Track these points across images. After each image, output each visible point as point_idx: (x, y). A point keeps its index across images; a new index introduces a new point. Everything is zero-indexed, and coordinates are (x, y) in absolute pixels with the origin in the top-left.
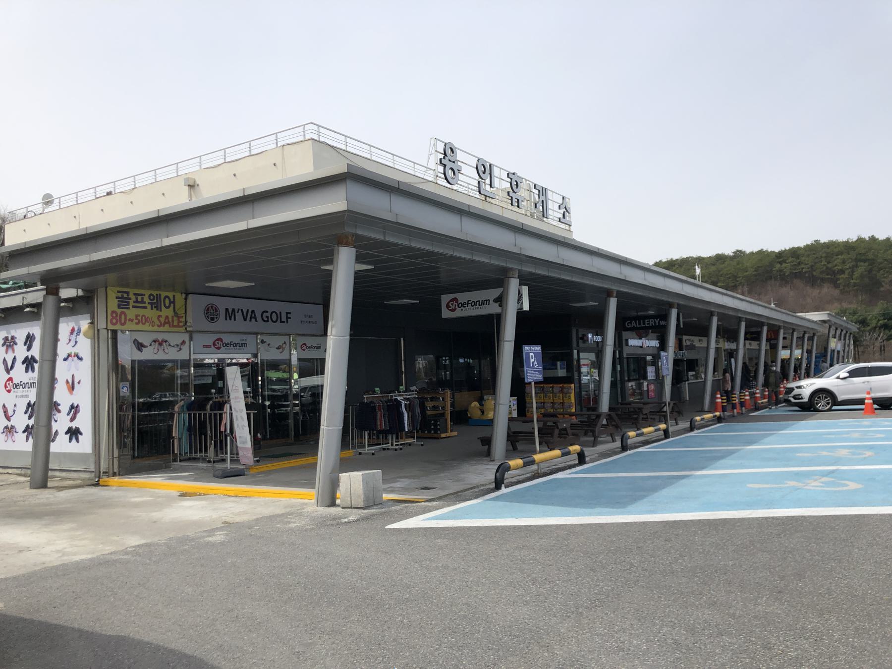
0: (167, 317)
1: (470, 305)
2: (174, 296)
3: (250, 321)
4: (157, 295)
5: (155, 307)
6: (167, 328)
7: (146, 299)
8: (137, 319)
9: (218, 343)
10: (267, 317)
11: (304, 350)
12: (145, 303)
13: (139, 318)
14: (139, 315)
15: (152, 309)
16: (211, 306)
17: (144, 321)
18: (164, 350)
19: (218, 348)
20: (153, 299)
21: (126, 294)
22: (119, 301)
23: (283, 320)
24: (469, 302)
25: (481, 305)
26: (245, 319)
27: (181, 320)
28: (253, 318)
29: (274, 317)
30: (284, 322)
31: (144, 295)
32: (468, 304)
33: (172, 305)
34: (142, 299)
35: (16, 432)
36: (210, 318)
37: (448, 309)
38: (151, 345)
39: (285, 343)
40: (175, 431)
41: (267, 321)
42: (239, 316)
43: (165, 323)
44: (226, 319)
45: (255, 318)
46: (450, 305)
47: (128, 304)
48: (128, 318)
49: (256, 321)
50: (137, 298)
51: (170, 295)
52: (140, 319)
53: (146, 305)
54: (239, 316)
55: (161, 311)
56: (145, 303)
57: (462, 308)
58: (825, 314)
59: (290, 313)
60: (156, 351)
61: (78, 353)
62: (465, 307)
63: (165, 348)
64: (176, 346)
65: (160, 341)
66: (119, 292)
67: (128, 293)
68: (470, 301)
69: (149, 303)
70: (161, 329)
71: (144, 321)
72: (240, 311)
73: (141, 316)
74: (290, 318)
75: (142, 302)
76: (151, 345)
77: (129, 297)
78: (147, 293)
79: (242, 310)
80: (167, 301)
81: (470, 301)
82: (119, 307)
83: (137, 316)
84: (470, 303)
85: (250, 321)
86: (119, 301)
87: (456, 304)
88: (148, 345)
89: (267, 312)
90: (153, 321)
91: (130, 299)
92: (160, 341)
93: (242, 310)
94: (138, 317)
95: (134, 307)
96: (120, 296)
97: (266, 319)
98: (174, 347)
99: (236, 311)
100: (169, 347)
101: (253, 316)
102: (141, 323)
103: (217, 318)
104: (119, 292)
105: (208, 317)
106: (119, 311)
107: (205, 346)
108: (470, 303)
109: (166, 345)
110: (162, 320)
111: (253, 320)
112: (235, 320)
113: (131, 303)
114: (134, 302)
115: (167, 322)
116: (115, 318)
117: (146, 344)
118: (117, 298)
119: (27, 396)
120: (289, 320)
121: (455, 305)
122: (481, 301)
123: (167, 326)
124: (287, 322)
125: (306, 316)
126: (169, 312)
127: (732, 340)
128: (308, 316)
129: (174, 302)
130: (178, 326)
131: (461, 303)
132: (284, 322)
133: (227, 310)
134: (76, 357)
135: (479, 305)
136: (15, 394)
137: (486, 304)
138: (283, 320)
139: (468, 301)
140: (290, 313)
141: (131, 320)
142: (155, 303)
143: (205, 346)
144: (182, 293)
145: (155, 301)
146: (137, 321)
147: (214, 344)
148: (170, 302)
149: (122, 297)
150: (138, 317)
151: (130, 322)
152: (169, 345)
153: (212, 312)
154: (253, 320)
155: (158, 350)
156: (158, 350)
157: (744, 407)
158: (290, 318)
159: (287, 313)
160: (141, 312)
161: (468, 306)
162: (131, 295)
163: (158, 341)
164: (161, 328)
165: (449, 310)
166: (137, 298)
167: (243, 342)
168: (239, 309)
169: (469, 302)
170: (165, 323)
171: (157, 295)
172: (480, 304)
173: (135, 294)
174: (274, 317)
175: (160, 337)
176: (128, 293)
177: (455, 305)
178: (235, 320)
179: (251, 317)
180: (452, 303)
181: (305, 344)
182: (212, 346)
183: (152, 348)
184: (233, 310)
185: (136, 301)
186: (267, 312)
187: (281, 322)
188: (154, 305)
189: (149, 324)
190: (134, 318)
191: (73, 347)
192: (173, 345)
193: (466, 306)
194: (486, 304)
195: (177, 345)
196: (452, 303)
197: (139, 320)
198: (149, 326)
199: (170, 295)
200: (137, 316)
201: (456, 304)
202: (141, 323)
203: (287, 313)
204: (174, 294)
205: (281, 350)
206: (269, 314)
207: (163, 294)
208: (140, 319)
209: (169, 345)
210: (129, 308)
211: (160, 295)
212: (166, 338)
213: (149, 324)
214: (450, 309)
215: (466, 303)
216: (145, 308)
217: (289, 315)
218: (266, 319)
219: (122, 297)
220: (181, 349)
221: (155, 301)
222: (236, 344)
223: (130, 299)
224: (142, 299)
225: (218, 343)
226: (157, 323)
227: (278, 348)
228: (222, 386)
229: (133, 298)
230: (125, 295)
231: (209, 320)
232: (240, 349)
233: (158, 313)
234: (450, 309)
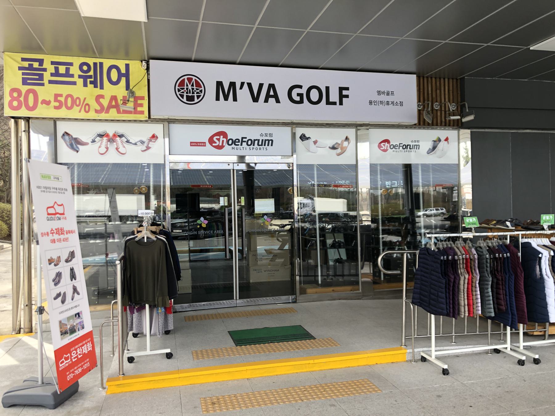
0: (114, 98)
1: (244, 144)
2: (127, 66)
3: (266, 101)
4: (95, 64)
5: (91, 83)
6: (113, 114)
7: (75, 70)
8: (56, 100)
9: (219, 140)
10: (300, 95)
11: (385, 151)
12: (72, 76)
13: (62, 99)
14: (61, 95)
15: (85, 85)
16: (188, 79)
17: (69, 104)
18: (117, 149)
19: (220, 147)
20: (89, 70)
21: (38, 63)
22: (23, 74)
23: (331, 100)
25: (262, 145)
26: (255, 99)
27: (139, 102)
28: (272, 96)
29: (314, 95)
30: (334, 103)
31: (71, 64)
32: (400, 146)
33: (123, 80)
34: (67, 70)
36: (185, 97)
38: (93, 141)
39: (347, 139)
40: (182, 248)
41: (301, 102)
42: (244, 94)
43: (110, 106)
44: (218, 99)
45: (276, 97)
47: (41, 77)
48: (40, 100)
49: (278, 101)
50: (57, 69)
51: (121, 64)
52: (63, 101)
53: (76, 79)
54: (244, 94)
55: (102, 88)
56: (72, 76)
59: (347, 89)
60: (103, 150)
62: (238, 145)
63: (120, 146)
64: (139, 143)
65: (111, 135)
66: (23, 60)
67: (41, 62)
69: (80, 77)
70: (103, 116)
71: (69, 104)
72: (246, 86)
73: (64, 96)
74: (347, 96)
75: (68, 74)
76: (93, 141)
77: (44, 67)
78: (77, 61)
79: (249, 85)
80: (114, 75)
82: (25, 82)
83: (56, 96)
85: (266, 101)
86: (23, 74)
88: (89, 141)
89: (300, 87)
90: (87, 104)
91: (45, 70)
92: (111, 135)
93: (249, 85)
94: (59, 98)
95: (50, 82)
96: (27, 66)
97: (298, 99)
98: (136, 144)
99: (238, 86)
100: (126, 145)
101: (272, 93)
102: (64, 107)
103: (198, 97)
104: (23, 60)
105: (182, 96)
106: (24, 89)
107: (193, 144)
109: (122, 142)
110: (105, 102)
111: (272, 100)
112: (235, 99)
113: (47, 76)
114: (52, 75)
115: (114, 104)
116: (17, 99)
117: (83, 139)
118: (20, 68)
120: (344, 99)
122: (415, 148)
123: (113, 111)
124: (341, 103)
125: (379, 93)
126: (120, 91)
128: (383, 93)
129: (127, 75)
130: (136, 112)
132: (334, 103)
133: (219, 84)
135: (258, 145)
137: (268, 145)
138: (331, 100)
140: (347, 89)
141: (48, 103)
142: (90, 77)
143: (193, 144)
144: (142, 61)
145: (91, 73)
146: (57, 104)
147: (211, 141)
148: (120, 75)
149: (31, 67)
150: (59, 98)
151: (44, 105)
152: (128, 142)
153: (190, 87)
154: (272, 100)
155: (107, 148)
156: (107, 148)
158: (347, 96)
159: (341, 89)
160: (64, 90)
161: (241, 145)
162: (47, 65)
163: (107, 135)
164: (101, 114)
165: (214, 147)
166: (57, 69)
167: (267, 138)
168: (243, 84)
170: (110, 106)
171: (95, 64)
172: (260, 144)
173: (53, 63)
174: (314, 95)
175: (111, 129)
176: (41, 62)
178: (235, 99)
179: (268, 97)
181: (387, 141)
182: (208, 144)
183: (97, 145)
184: (232, 85)
185: (57, 73)
186: (300, 87)
187: (328, 103)
188: (89, 80)
189: (79, 108)
190: (52, 99)
192: (134, 142)
193: (398, 148)
194: (268, 145)
195: (142, 142)
197: (60, 102)
198: (80, 112)
199: (121, 64)
200: (56, 96)
202: (64, 107)
203: (341, 89)
204: (127, 62)
205: (339, 151)
206: (304, 91)
207: (107, 63)
208: (63, 101)
209: (128, 142)
210: (43, 85)
211: (101, 64)
212: (121, 132)
213: (79, 108)
214: (381, 149)
216: (74, 83)
217: (345, 93)
218: (298, 99)
219: (31, 67)
220: (148, 148)
221: (91, 73)
222: (253, 142)
223: (45, 70)
224: (67, 70)
225: (219, 140)
226: (94, 105)
227: (333, 148)
228: (226, 204)
229: (51, 69)
230: (36, 65)
231: (185, 100)
232: (260, 149)
233: (98, 91)
234: (381, 149)
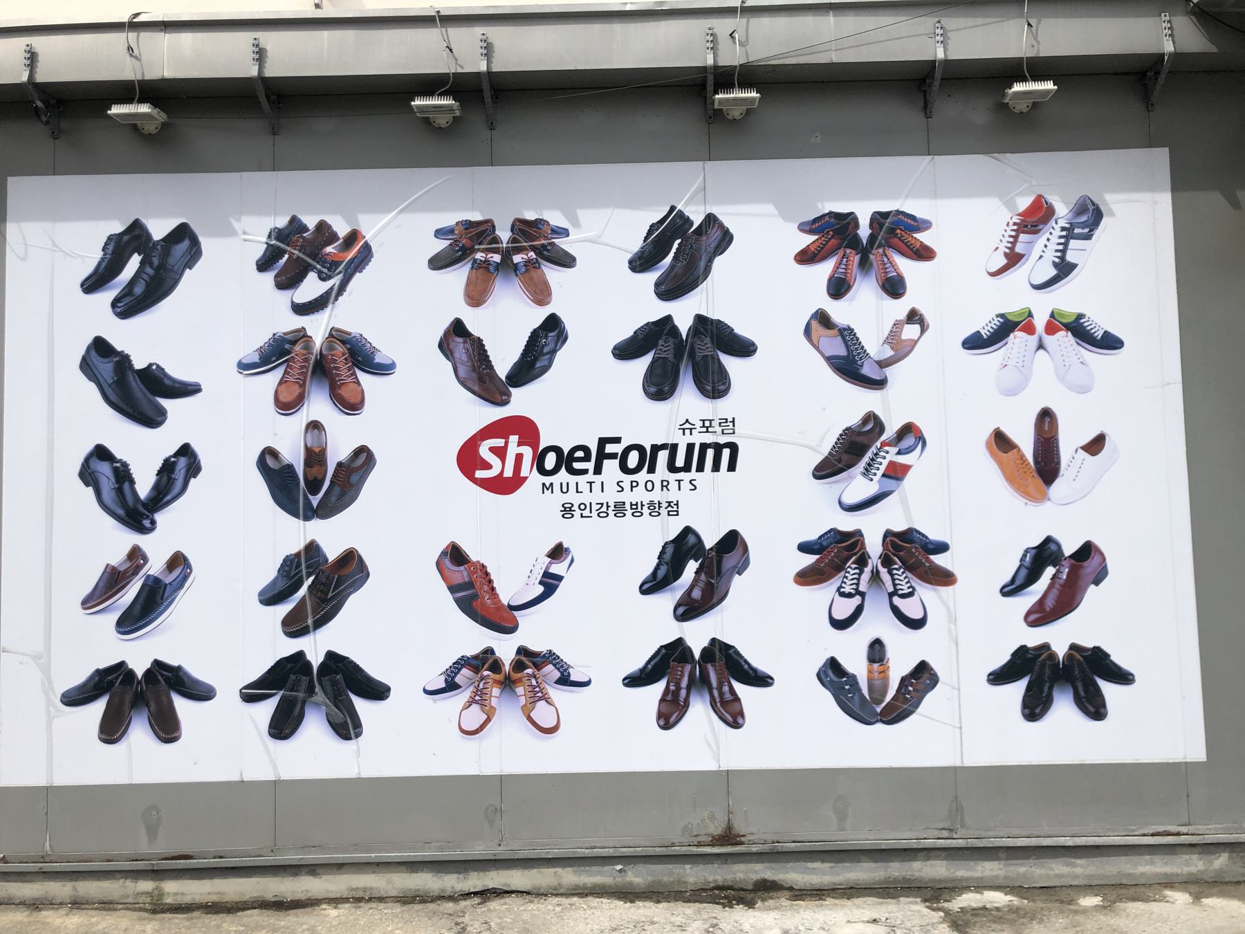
1: (611, 466)
24: (610, 448)
32: (602, 456)
35: (565, 680)
37: (469, 475)
46: (484, 451)
57: (563, 474)
58: (188, 688)
61: (1080, 316)
62: (585, 472)
68: (617, 440)
81: (617, 440)
84: (613, 456)
87: (527, 452)
108: (613, 456)
119: (673, 509)
121: (519, 458)
127: (1027, 711)
131: (557, 450)
134: (1064, 339)
135: (672, 468)
136: (558, 499)
137: (716, 467)
139: (603, 442)
157: (1192, 903)
161: (598, 470)
167: (708, 438)
169: (610, 448)
172: (680, 462)
177: (519, 458)
180: (499, 442)
191: (994, 274)
193: (590, 466)
194: (716, 467)
196: (499, 442)
201: (527, 452)
214: (480, 474)
215: (585, 449)
234: (480, 474)
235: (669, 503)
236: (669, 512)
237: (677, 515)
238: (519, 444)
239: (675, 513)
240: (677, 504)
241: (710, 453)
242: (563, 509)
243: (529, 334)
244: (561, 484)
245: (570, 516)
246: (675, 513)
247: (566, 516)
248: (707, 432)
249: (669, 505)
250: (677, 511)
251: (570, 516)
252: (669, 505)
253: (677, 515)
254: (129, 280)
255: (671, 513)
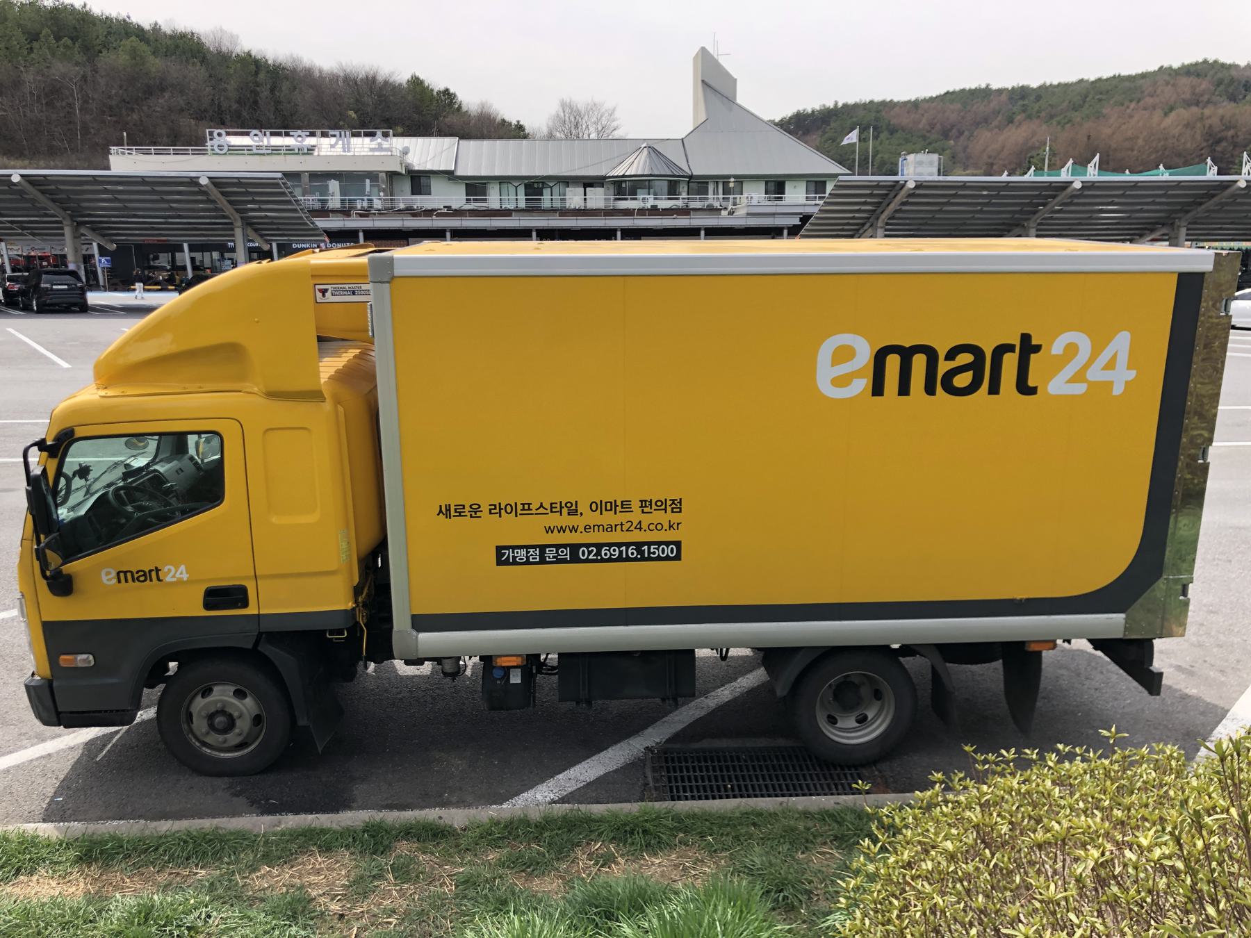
137: (904, 389)
194: (904, 389)
235: (673, 500)
236: (673, 508)
237: (680, 512)
238: (1109, 384)
239: (678, 510)
240: (680, 503)
241: (893, 362)
242: (503, 506)
243: (1211, 59)
244: (441, 506)
245: (473, 507)
246: (678, 510)
247: (477, 506)
248: (460, 515)
249: (673, 503)
250: (680, 509)
251: (473, 507)
252: (673, 503)
253: (680, 512)
254: (46, 658)
255: (675, 510)
